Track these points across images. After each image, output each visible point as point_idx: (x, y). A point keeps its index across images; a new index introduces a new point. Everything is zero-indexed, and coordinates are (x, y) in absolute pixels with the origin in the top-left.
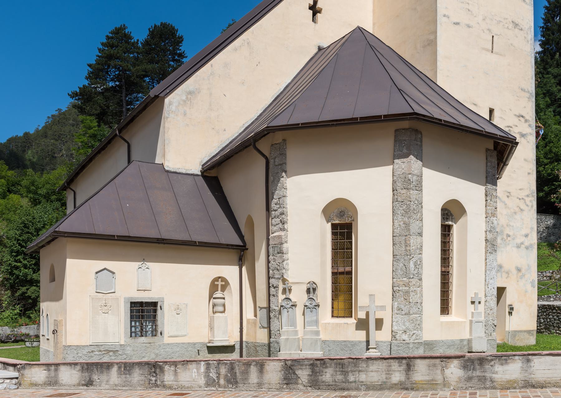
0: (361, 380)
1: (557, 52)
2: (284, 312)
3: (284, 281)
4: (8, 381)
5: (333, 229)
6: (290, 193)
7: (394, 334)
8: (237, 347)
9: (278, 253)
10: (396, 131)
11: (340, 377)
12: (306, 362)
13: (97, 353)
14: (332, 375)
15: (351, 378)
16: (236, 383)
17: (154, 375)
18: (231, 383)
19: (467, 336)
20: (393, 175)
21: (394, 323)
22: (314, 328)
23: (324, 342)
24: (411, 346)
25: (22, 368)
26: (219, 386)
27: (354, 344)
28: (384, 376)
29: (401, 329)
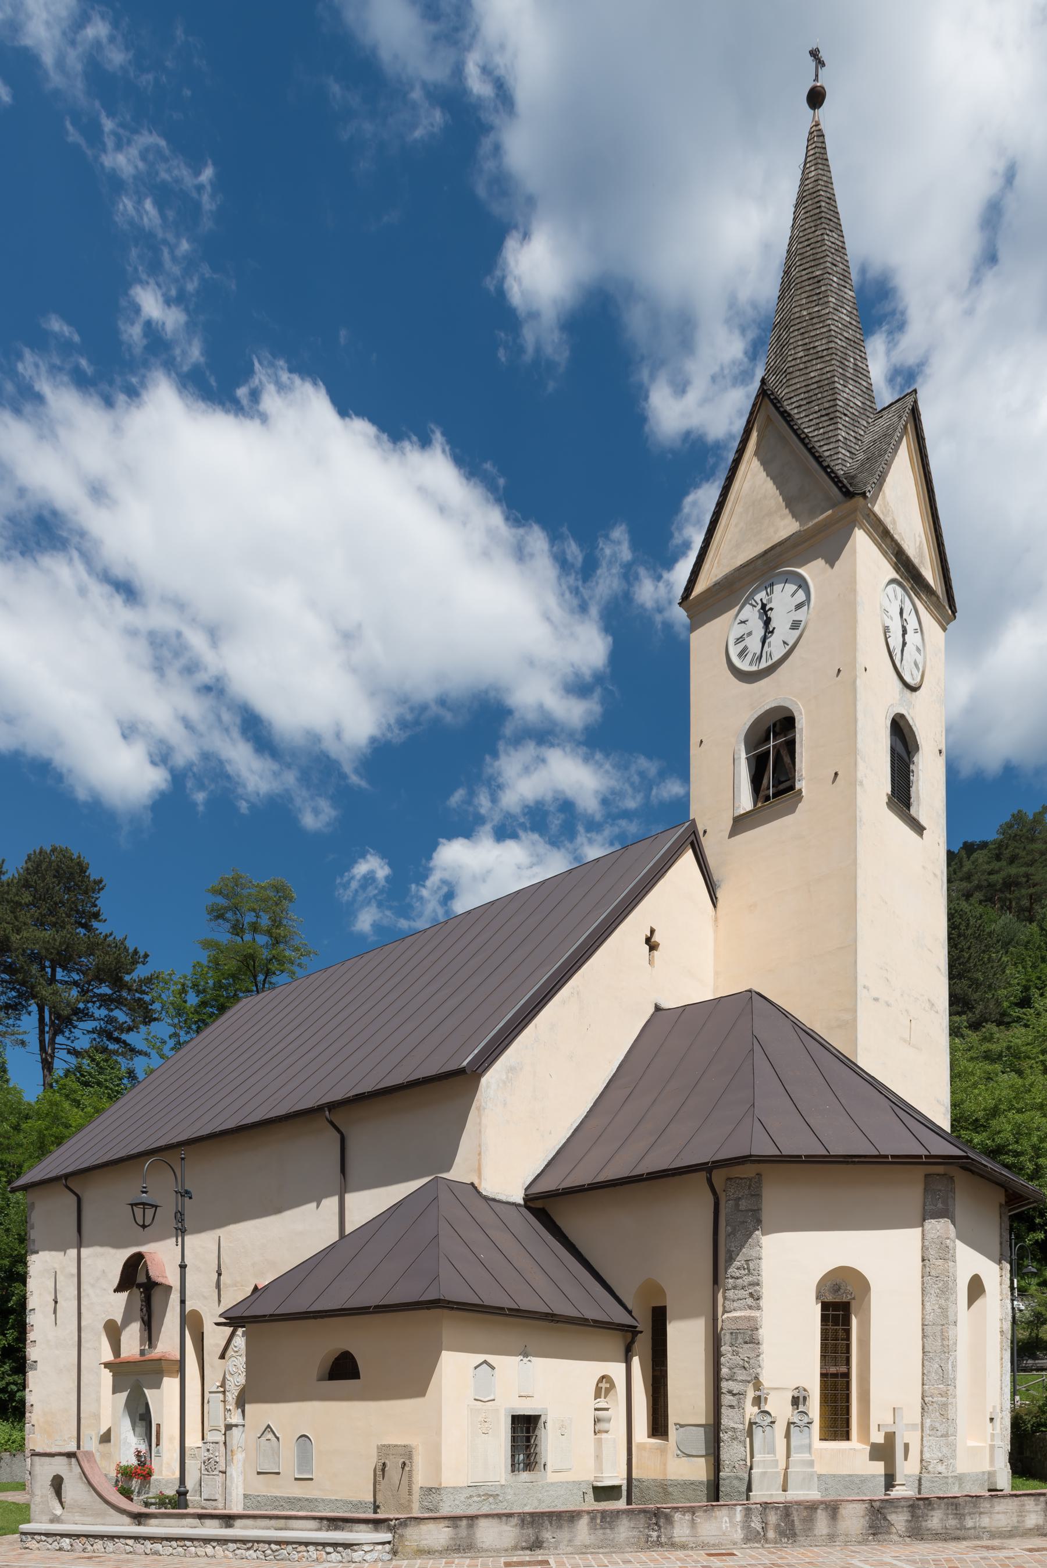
0: (983, 1525)
1: (362, 937)
2: (758, 1433)
3: (757, 1385)
4: (380, 1547)
5: (822, 1310)
6: (765, 1253)
7: (925, 1464)
8: (624, 1488)
9: (746, 1343)
10: (927, 1176)
11: (952, 1522)
12: (903, 1503)
13: (475, 1499)
14: (941, 1520)
15: (969, 1523)
16: (794, 1535)
17: (656, 1527)
18: (786, 1536)
19: (987, 1468)
20: (923, 1238)
21: (925, 1449)
22: (806, 1456)
23: (820, 1476)
24: (950, 1480)
25: (401, 1524)
26: (767, 1541)
27: (864, 1479)
28: (1015, 1519)
29: (935, 1456)
